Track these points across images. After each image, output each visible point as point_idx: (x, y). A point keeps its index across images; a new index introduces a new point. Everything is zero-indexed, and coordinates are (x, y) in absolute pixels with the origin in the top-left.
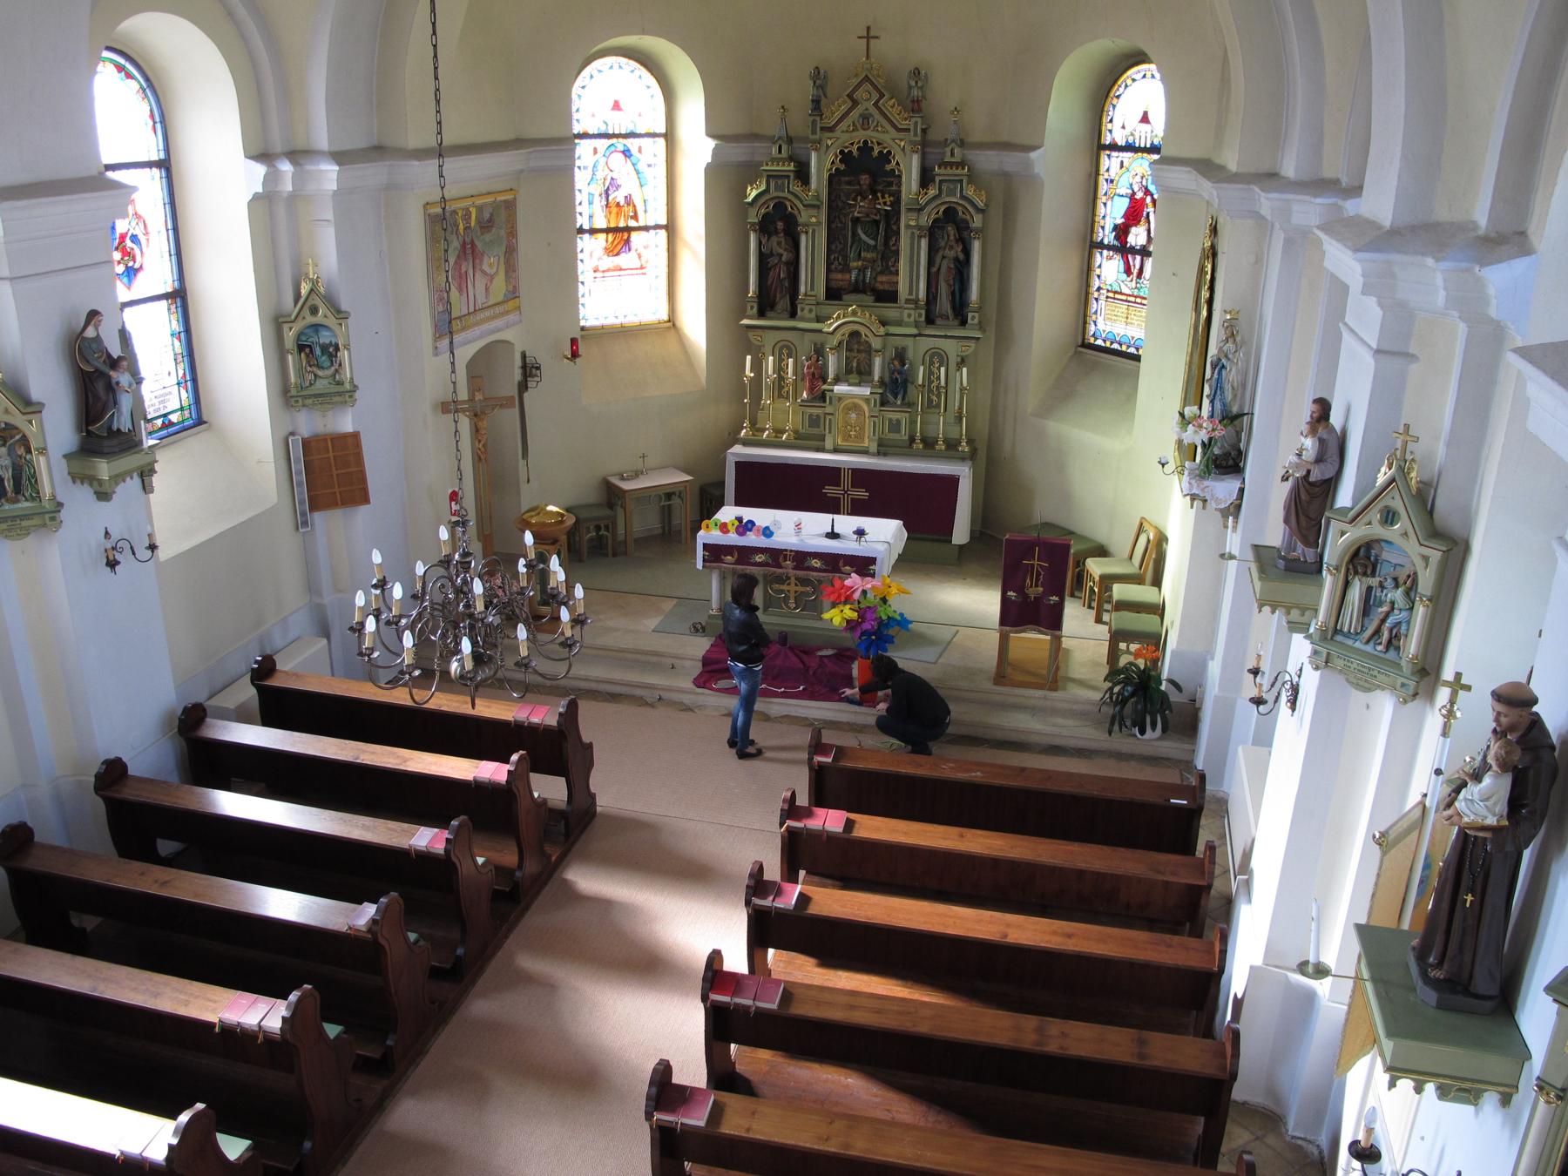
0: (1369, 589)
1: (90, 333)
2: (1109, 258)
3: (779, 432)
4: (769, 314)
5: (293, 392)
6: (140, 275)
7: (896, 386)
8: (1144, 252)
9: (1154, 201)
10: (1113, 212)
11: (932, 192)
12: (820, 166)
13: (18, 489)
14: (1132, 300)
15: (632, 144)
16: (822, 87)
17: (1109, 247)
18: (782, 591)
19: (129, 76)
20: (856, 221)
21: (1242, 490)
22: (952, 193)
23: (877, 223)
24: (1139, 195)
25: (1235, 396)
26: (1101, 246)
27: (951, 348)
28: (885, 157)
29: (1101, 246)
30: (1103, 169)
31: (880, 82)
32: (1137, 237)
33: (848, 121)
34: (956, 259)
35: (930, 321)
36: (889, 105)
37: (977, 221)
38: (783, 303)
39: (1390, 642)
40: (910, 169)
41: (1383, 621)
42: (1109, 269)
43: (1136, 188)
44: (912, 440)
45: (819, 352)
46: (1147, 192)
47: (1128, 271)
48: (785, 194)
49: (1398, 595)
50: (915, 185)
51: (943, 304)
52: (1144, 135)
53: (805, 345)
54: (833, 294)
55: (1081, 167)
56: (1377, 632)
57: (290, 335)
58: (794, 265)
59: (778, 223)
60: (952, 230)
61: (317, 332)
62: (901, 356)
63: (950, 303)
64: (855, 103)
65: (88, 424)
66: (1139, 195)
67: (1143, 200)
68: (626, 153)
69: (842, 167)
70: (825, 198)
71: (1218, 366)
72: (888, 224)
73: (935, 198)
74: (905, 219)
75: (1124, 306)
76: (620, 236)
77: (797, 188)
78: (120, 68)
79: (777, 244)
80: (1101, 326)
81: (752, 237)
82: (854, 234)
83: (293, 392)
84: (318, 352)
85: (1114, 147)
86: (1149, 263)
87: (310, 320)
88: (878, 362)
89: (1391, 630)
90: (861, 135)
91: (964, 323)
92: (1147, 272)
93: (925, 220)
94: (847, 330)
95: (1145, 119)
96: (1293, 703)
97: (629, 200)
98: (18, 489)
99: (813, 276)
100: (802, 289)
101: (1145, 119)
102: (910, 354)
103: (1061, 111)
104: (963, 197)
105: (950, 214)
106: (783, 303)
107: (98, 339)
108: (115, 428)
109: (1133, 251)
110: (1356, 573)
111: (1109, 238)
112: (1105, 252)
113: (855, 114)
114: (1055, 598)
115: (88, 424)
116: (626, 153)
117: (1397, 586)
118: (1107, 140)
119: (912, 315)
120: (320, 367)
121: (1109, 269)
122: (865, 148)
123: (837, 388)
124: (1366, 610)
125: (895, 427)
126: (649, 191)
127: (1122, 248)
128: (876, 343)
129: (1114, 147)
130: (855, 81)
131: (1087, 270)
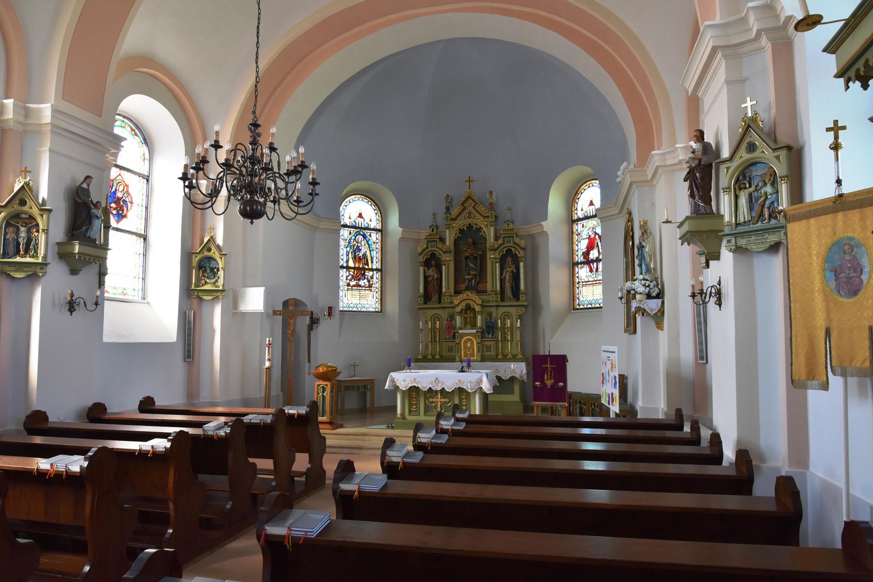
0: (750, 195)
1: (85, 186)
2: (582, 268)
3: (433, 356)
5: (193, 287)
6: (124, 220)
7: (490, 328)
8: (598, 260)
9: (600, 237)
10: (583, 245)
11: (500, 242)
12: (450, 237)
13: (27, 251)
14: (595, 283)
15: (367, 233)
16: (451, 202)
17: (581, 263)
18: (433, 402)
19: (136, 134)
20: (467, 258)
21: (663, 303)
22: (509, 242)
23: (476, 258)
24: (592, 236)
25: (651, 259)
26: (578, 263)
27: (513, 311)
28: (479, 229)
29: (578, 263)
30: (575, 230)
31: (475, 198)
32: (594, 254)
33: (462, 215)
34: (513, 272)
35: (502, 300)
36: (481, 208)
37: (520, 254)
38: (435, 298)
39: (770, 216)
41: (763, 206)
42: (583, 273)
44: (497, 355)
45: (452, 318)
46: (596, 234)
47: (591, 271)
48: (512, 244)
49: (769, 189)
50: (492, 240)
51: (508, 292)
52: (591, 210)
53: (444, 314)
54: (457, 292)
55: (564, 230)
56: (761, 214)
57: (195, 260)
59: (432, 261)
60: (509, 258)
61: (209, 261)
62: (490, 315)
63: (513, 290)
64: (465, 208)
65: (73, 230)
66: (592, 236)
67: (594, 238)
68: (364, 236)
70: (452, 248)
71: (641, 247)
72: (481, 261)
73: (501, 245)
74: (491, 256)
75: (591, 287)
76: (360, 273)
77: (440, 245)
78: (132, 130)
79: (432, 272)
80: (581, 299)
82: (467, 264)
83: (193, 287)
84: (208, 271)
85: (579, 219)
86: (600, 265)
87: (206, 254)
88: (479, 317)
89: (769, 208)
90: (468, 221)
91: (518, 300)
92: (600, 269)
93: (497, 255)
95: (591, 204)
96: (719, 303)
97: (365, 255)
98: (27, 251)
99: (448, 285)
100: (444, 290)
101: (591, 204)
102: (494, 315)
103: (555, 204)
104: (514, 243)
105: (509, 251)
106: (435, 298)
107: (87, 191)
108: (88, 235)
109: (593, 261)
110: (740, 189)
111: (580, 258)
113: (465, 213)
114: (561, 384)
115: (73, 230)
116: (364, 236)
117: (765, 184)
118: (575, 217)
119: (493, 298)
120: (208, 278)
121: (583, 273)
122: (470, 227)
123: (460, 331)
124: (751, 209)
125: (489, 349)
126: (374, 253)
127: (588, 262)
128: (478, 308)
129: (579, 219)
130: (463, 199)
131: (573, 275)
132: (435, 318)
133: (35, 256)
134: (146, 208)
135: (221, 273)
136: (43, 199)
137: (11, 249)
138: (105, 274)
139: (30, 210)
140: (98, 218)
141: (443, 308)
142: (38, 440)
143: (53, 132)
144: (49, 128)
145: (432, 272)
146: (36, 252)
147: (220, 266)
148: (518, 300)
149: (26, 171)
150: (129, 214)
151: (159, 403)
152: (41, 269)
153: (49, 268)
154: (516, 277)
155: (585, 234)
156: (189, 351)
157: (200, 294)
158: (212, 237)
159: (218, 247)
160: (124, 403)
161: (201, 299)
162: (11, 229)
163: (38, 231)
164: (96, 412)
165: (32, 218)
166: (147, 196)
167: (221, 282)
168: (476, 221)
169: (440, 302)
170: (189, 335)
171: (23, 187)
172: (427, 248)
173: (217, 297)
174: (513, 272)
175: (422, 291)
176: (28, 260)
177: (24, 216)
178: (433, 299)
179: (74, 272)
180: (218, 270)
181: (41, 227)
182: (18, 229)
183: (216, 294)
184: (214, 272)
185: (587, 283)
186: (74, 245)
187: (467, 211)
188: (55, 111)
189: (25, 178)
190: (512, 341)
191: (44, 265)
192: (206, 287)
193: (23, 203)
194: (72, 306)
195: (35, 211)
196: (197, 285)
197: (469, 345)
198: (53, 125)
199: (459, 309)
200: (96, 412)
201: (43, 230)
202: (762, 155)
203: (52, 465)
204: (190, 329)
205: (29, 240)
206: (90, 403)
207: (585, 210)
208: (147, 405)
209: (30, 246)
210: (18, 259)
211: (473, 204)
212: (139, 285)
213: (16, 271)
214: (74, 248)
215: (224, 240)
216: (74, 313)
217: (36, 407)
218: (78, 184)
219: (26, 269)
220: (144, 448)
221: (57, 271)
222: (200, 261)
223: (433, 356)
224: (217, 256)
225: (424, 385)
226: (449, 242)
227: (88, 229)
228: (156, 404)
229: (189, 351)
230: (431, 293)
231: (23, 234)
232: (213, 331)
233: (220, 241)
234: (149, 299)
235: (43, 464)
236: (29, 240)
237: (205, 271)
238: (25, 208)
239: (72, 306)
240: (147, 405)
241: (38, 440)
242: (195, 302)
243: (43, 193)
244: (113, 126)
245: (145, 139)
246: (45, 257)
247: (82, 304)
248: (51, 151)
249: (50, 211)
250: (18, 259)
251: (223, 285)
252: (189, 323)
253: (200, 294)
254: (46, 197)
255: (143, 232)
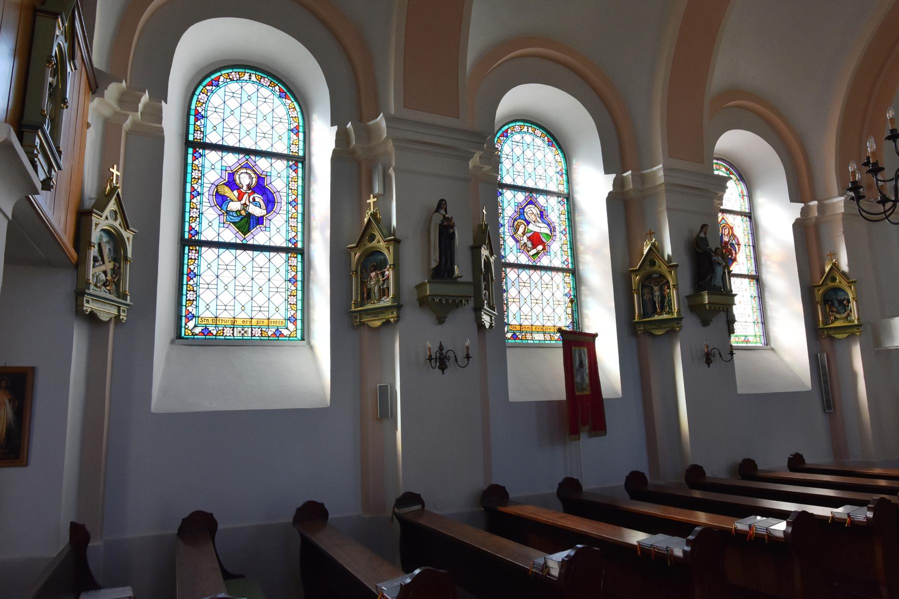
1: (702, 235)
5: (821, 326)
13: (662, 308)
57: (819, 293)
83: (821, 326)
84: (836, 304)
120: (838, 312)
133: (670, 312)
134: (754, 247)
135: (853, 305)
136: (668, 256)
137: (649, 309)
138: (734, 321)
139: (660, 269)
140: (719, 264)
142: (697, 494)
143: (667, 191)
144: (663, 188)
146: (670, 308)
147: (851, 296)
149: (651, 234)
150: (738, 259)
151: (809, 460)
152: (678, 323)
153: (683, 322)
156: (828, 401)
157: (831, 332)
158: (834, 264)
159: (843, 273)
160: (772, 460)
161: (832, 339)
162: (646, 290)
163: (669, 288)
164: (747, 468)
165: (662, 276)
166: (753, 234)
167: (855, 316)
170: (826, 382)
171: (650, 249)
173: (853, 334)
176: (665, 316)
177: (655, 276)
179: (705, 323)
180: (849, 302)
181: (671, 283)
182: (652, 289)
183: (851, 331)
184: (844, 305)
186: (703, 296)
188: (666, 169)
189: (651, 240)
191: (679, 320)
192: (837, 324)
193: (653, 263)
194: (708, 359)
195: (664, 269)
196: (826, 322)
198: (666, 183)
200: (747, 468)
201: (674, 286)
202: (377, 245)
203: (750, 526)
204: (825, 375)
205: (663, 297)
206: (740, 460)
208: (796, 462)
209: (665, 303)
210: (656, 317)
212: (759, 330)
213: (656, 329)
214: (703, 299)
215: (849, 265)
216: (711, 365)
217: (692, 461)
218: (695, 235)
219: (664, 326)
220: (837, 516)
221: (690, 323)
222: (825, 294)
224: (844, 285)
227: (711, 278)
228: (806, 462)
229: (828, 401)
231: (657, 293)
232: (854, 375)
233: (844, 265)
235: (741, 525)
236: (663, 297)
237: (832, 305)
238: (656, 268)
239: (708, 359)
240: (796, 462)
241: (697, 494)
242: (826, 343)
243: (668, 250)
244: (713, 170)
245: (740, 176)
246: (679, 312)
247: (717, 355)
248: (668, 209)
249: (676, 266)
250: (656, 317)
251: (859, 319)
252: (823, 367)
253: (831, 332)
254: (670, 253)
255: (754, 273)
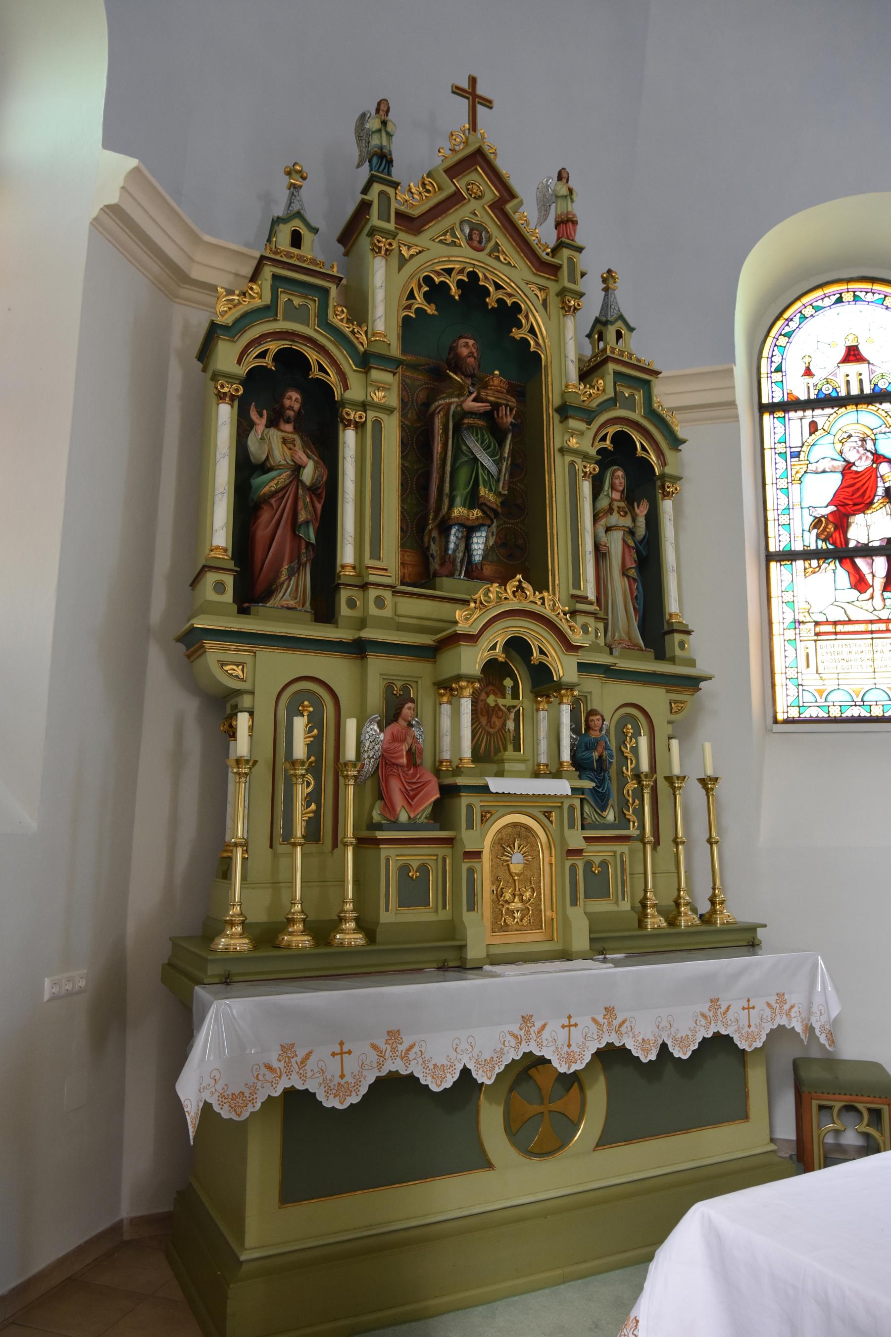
3: (322, 931)
4: (259, 608)
10: (821, 492)
12: (386, 294)
17: (807, 555)
22: (630, 404)
26: (789, 556)
28: (510, 314)
29: (789, 556)
38: (294, 588)
40: (562, 344)
43: (852, 456)
47: (860, 583)
58: (328, 493)
59: (290, 391)
60: (635, 471)
64: (456, 199)
66: (862, 465)
69: (431, 310)
74: (571, 446)
75: (862, 644)
81: (225, 413)
85: (791, 405)
90: (463, 257)
94: (498, 636)
100: (347, 554)
112: (800, 564)
129: (791, 405)
132: (305, 696)
141: (359, 649)
145: (274, 444)
148: (661, 655)
154: (647, 560)
155: (824, 452)
168: (503, 274)
169: (325, 612)
172: (268, 311)
174: (631, 532)
175: (220, 533)
178: (284, 597)
185: (834, 628)
187: (463, 212)
190: (657, 843)
197: (517, 862)
199: (471, 660)
207: (820, 374)
211: (491, 193)
223: (322, 931)
225: (568, 1049)
226: (383, 321)
230: (278, 552)
234: (632, 325)
235: (559, 1272)
